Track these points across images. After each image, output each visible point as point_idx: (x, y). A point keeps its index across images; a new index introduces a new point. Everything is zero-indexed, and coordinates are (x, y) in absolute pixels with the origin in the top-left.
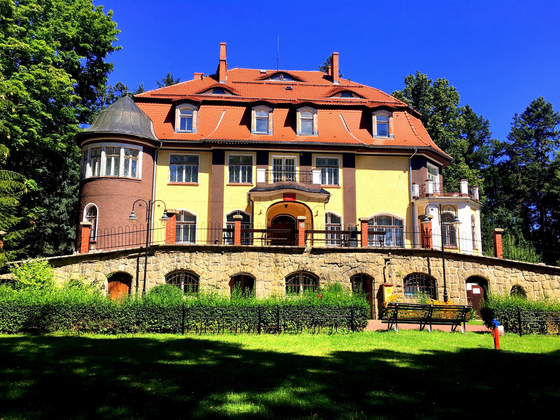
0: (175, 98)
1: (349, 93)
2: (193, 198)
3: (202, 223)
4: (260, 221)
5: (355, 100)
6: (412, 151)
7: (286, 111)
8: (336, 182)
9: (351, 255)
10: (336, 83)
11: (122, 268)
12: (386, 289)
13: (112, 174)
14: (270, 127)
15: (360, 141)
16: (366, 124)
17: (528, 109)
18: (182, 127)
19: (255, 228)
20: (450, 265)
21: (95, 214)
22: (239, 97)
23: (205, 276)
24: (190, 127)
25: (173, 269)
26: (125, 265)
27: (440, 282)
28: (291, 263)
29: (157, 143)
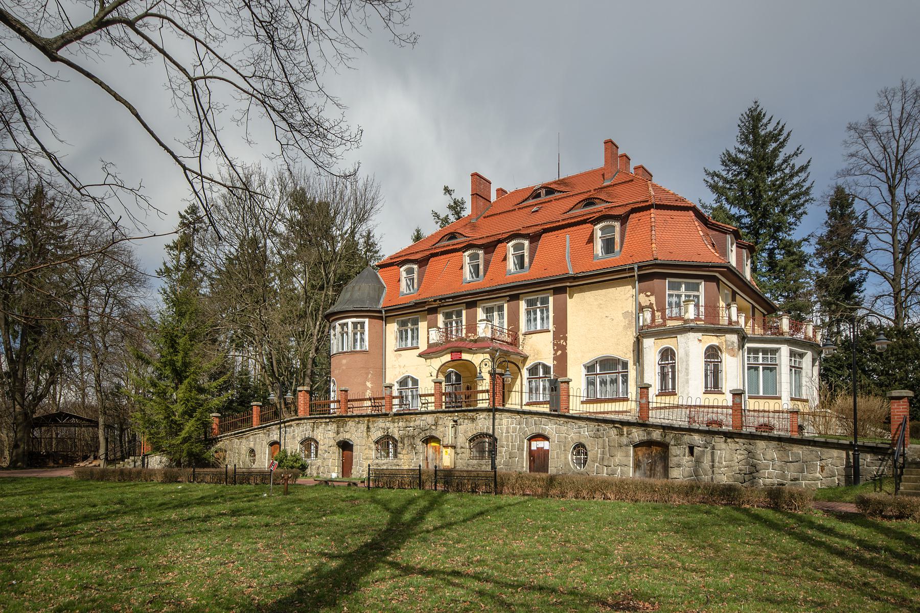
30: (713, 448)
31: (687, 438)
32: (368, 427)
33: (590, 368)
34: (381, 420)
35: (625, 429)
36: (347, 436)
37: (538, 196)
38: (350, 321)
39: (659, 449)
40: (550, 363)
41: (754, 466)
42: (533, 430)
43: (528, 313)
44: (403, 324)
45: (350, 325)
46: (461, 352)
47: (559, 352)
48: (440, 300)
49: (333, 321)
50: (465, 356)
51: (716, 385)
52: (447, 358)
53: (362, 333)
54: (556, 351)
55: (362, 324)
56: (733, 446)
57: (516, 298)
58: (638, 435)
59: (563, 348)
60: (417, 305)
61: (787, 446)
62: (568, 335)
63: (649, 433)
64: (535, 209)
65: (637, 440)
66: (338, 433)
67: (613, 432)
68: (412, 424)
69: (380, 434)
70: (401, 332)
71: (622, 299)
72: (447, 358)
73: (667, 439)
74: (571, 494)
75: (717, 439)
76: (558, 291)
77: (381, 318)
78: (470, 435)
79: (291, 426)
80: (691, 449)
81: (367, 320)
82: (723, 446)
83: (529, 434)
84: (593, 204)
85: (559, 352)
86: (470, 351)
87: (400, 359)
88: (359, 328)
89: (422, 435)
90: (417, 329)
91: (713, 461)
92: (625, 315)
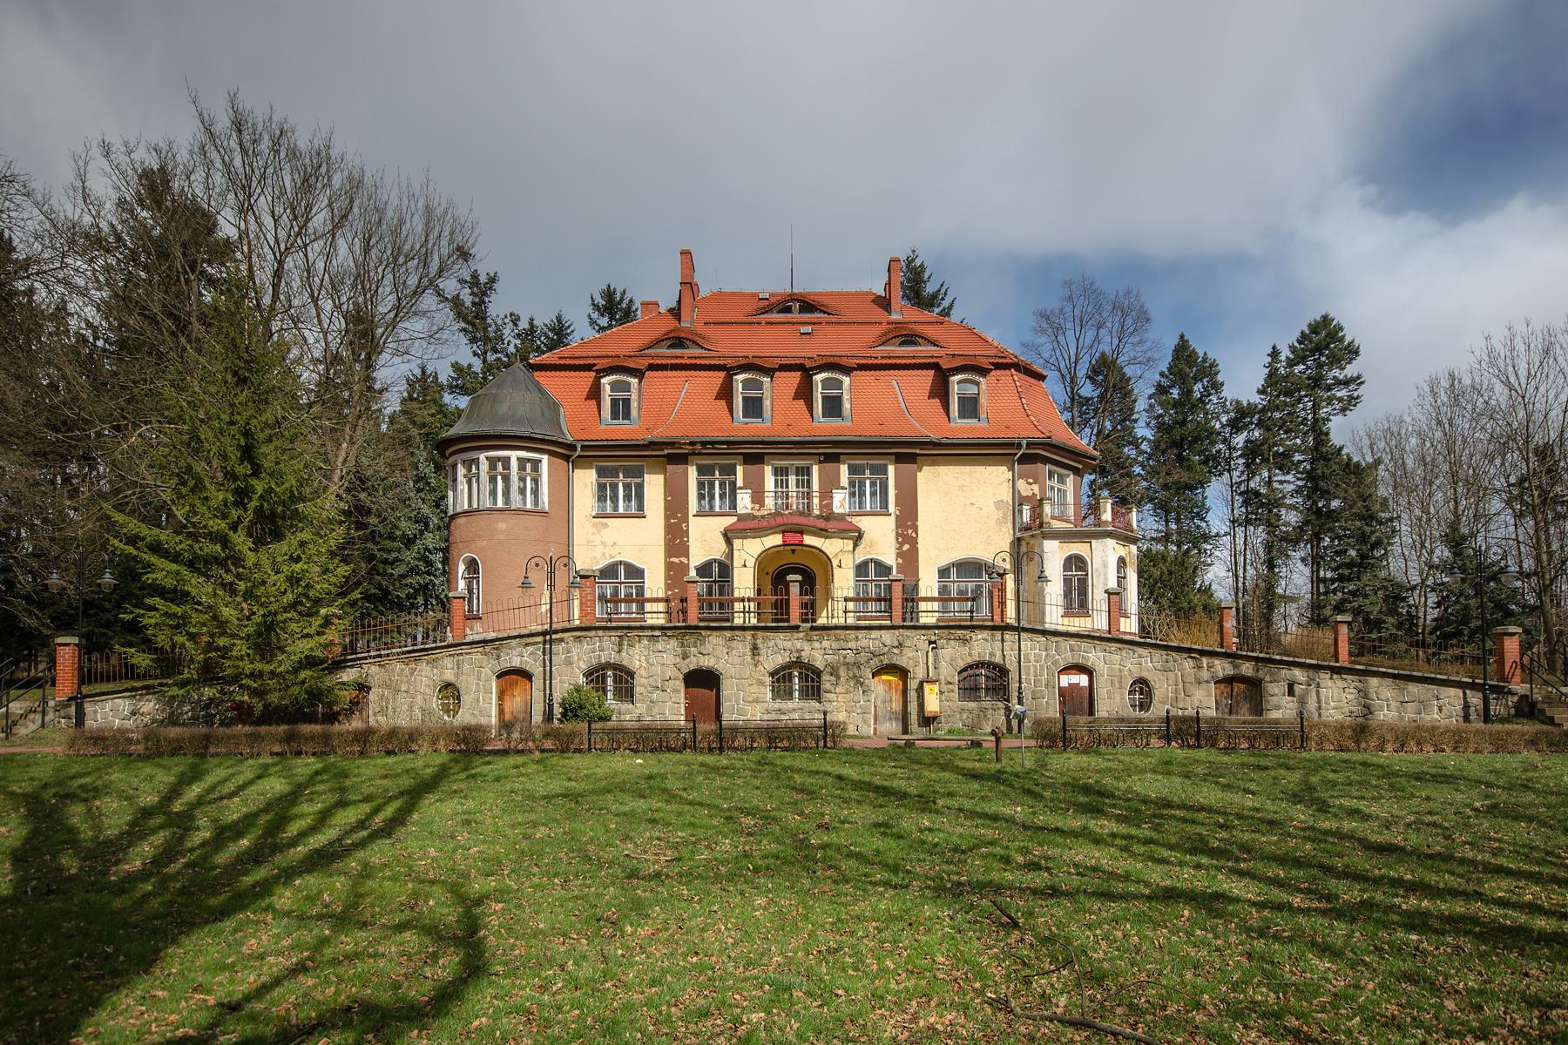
0: (730, 363)
1: (910, 339)
2: (637, 540)
3: (655, 584)
4: (744, 582)
5: (923, 351)
6: (1019, 446)
7: (796, 377)
8: (885, 504)
9: (875, 634)
10: (895, 317)
11: (516, 662)
12: (927, 687)
13: (500, 504)
14: (781, 412)
15: (926, 432)
16: (940, 391)
17: (1353, 352)
18: (615, 416)
19: (922, 594)
20: (1030, 645)
21: (476, 571)
22: (713, 354)
23: (643, 672)
24: (627, 416)
25: (594, 662)
26: (517, 657)
27: (1013, 676)
28: (779, 649)
29: (572, 447)
30: (1318, 686)
31: (1285, 673)
32: (755, 648)
33: (944, 572)
34: (781, 636)
35: (1205, 660)
36: (707, 662)
37: (788, 310)
38: (514, 455)
39: (1242, 686)
40: (890, 559)
41: (1367, 707)
42: (1070, 658)
43: (701, 485)
44: (601, 473)
45: (514, 464)
46: (802, 533)
47: (906, 547)
48: (704, 444)
49: (452, 454)
50: (809, 540)
51: (1083, 604)
52: (776, 540)
53: (536, 481)
54: (901, 545)
55: (536, 464)
56: (1340, 684)
57: (834, 459)
58: (1222, 668)
59: (913, 542)
60: (651, 445)
61: (1401, 683)
62: (919, 523)
63: (1236, 667)
64: (809, 329)
65: (1221, 675)
66: (685, 656)
67: (1188, 664)
68: (852, 645)
69: (780, 660)
70: (601, 487)
71: (992, 484)
72: (776, 540)
73: (1261, 674)
74: (1389, 747)
75: (1322, 676)
76: (900, 459)
77: (567, 458)
78: (961, 664)
79: (562, 640)
80: (1291, 687)
81: (545, 458)
82: (1330, 683)
83: (1062, 665)
84: (915, 344)
85: (906, 547)
86: (823, 533)
87: (604, 532)
88: (528, 469)
89: (875, 663)
90: (640, 487)
91: (1319, 701)
92: (999, 504)
